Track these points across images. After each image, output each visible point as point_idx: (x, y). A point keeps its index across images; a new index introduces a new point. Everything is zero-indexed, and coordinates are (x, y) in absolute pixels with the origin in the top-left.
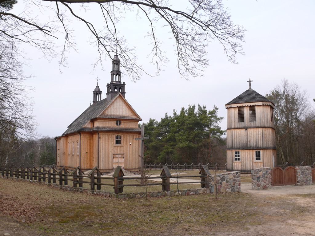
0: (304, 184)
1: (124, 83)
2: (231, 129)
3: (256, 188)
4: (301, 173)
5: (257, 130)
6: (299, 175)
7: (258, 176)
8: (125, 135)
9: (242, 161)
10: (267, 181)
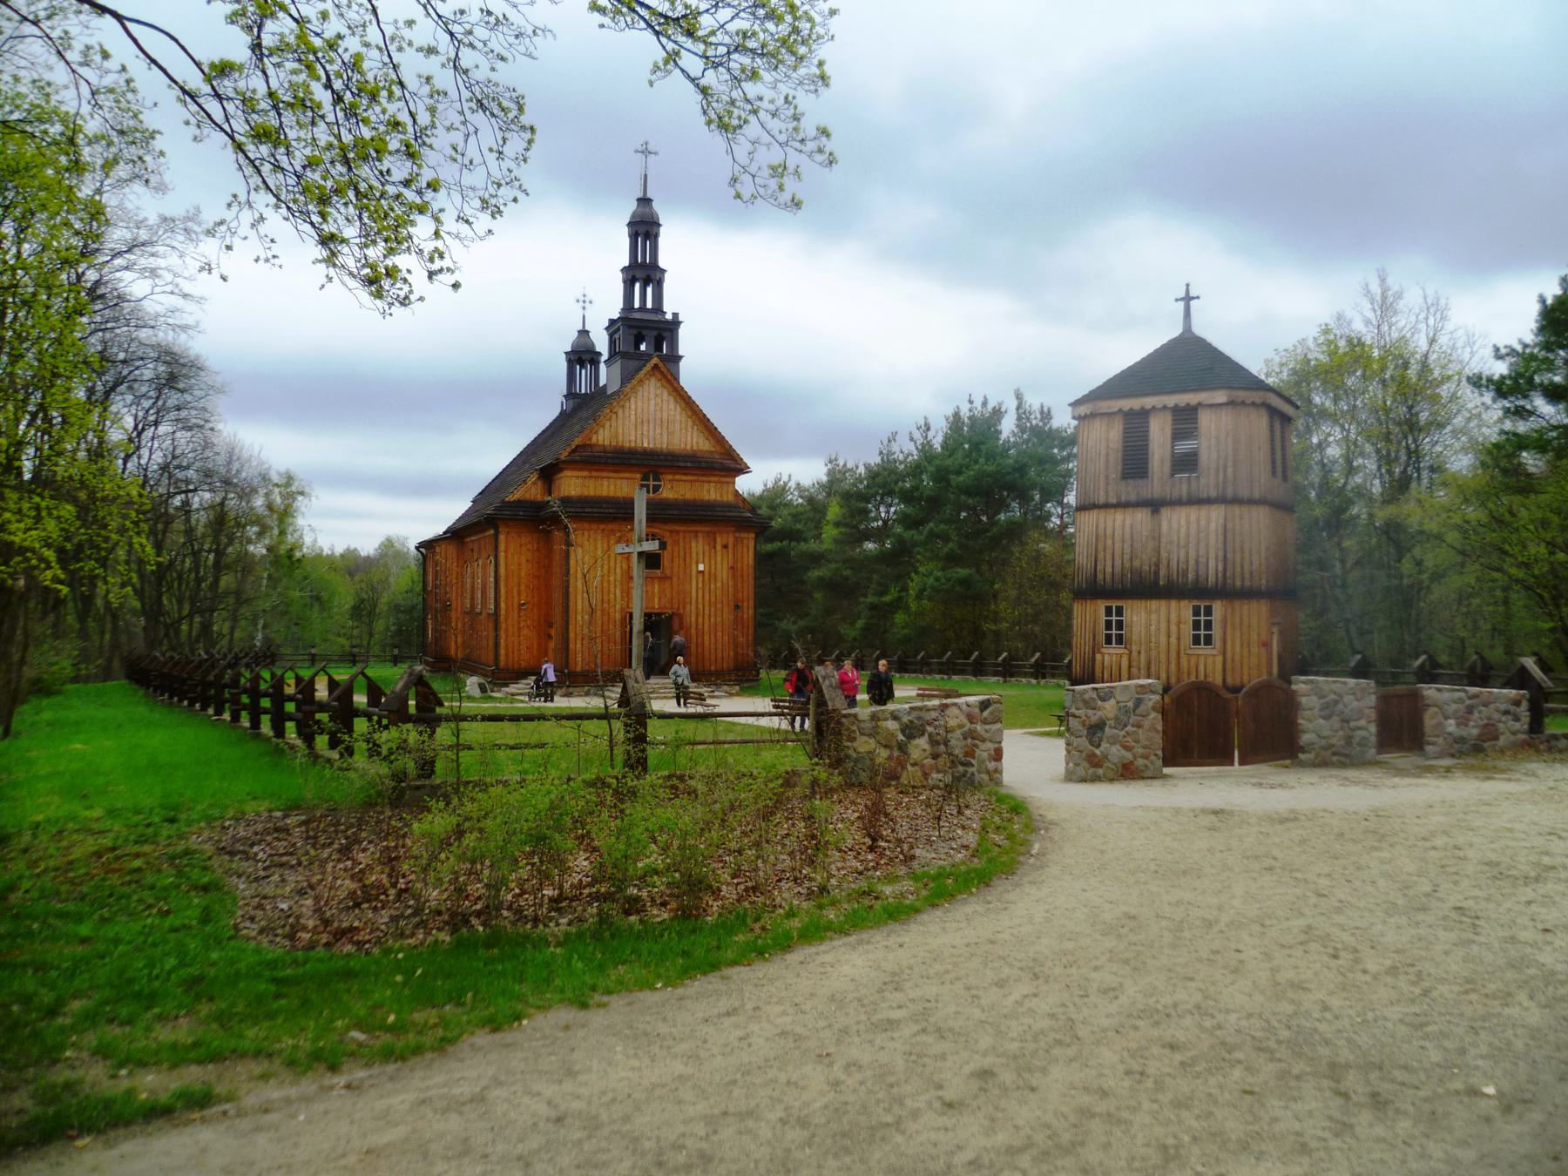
0: (1335, 758)
1: (675, 315)
2: (1095, 506)
3: (1081, 771)
4: (1322, 710)
5: (1204, 511)
6: (1310, 721)
7: (1094, 720)
8: (678, 532)
9: (1134, 647)
10: (1137, 741)
